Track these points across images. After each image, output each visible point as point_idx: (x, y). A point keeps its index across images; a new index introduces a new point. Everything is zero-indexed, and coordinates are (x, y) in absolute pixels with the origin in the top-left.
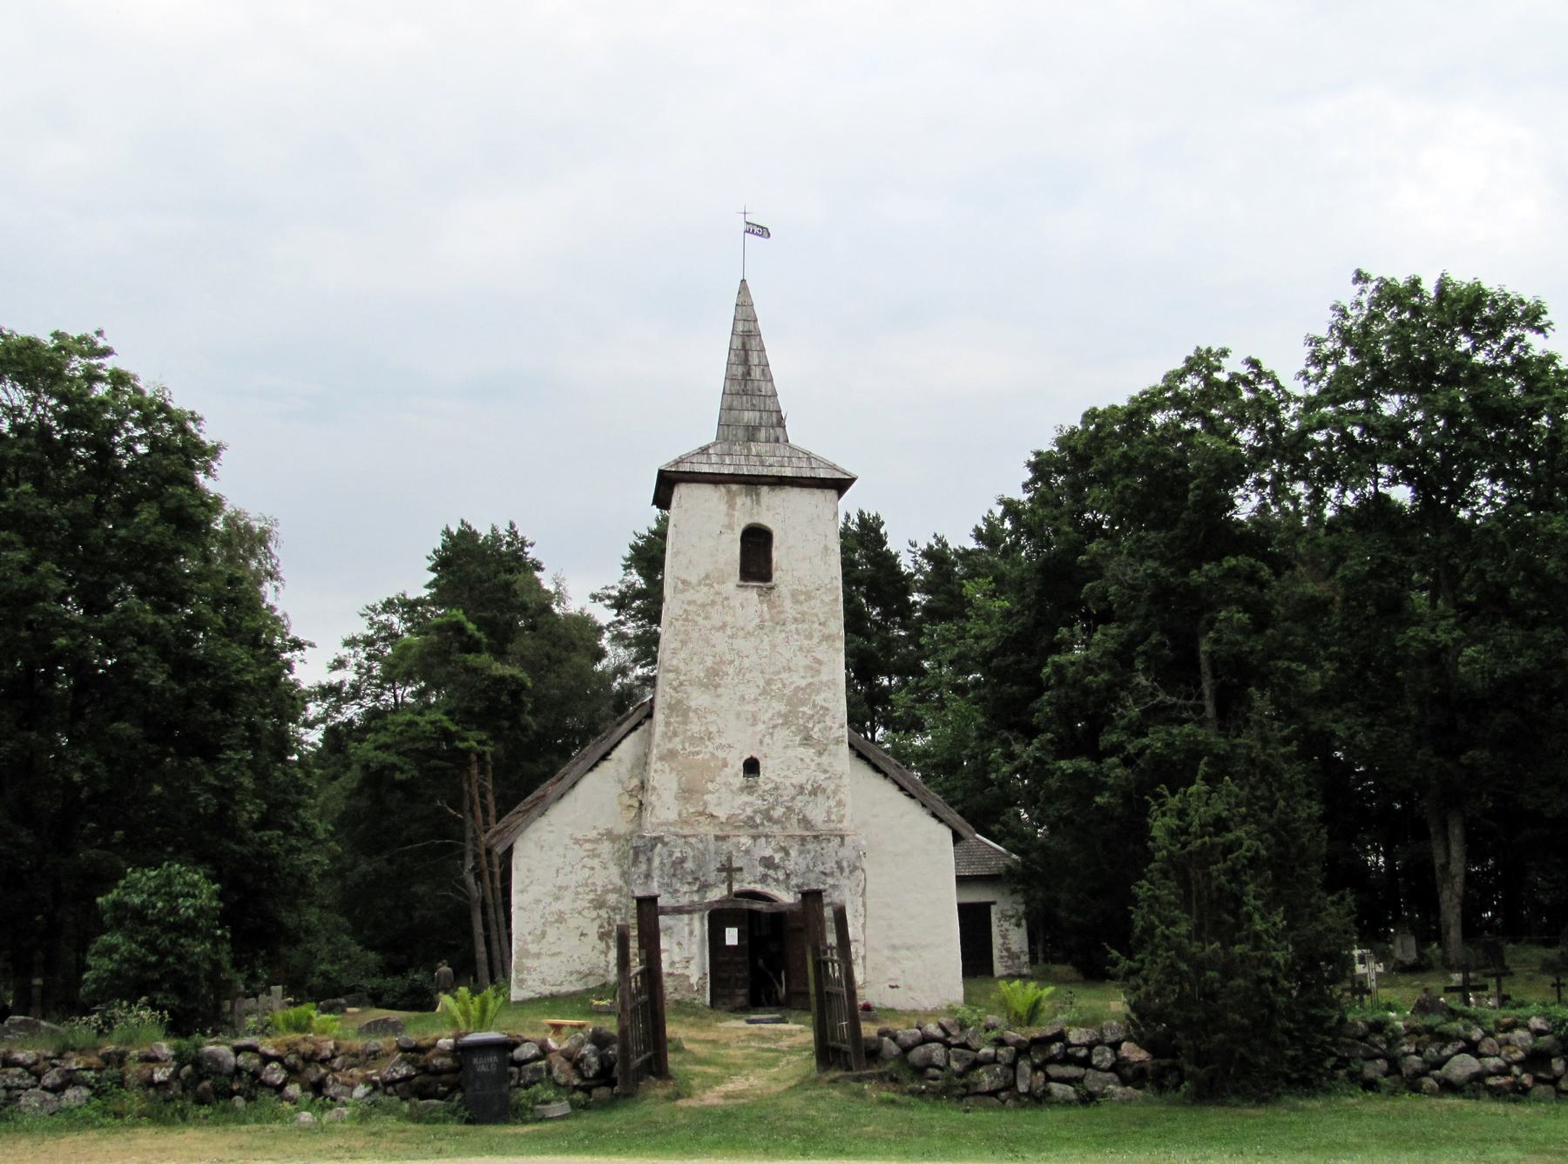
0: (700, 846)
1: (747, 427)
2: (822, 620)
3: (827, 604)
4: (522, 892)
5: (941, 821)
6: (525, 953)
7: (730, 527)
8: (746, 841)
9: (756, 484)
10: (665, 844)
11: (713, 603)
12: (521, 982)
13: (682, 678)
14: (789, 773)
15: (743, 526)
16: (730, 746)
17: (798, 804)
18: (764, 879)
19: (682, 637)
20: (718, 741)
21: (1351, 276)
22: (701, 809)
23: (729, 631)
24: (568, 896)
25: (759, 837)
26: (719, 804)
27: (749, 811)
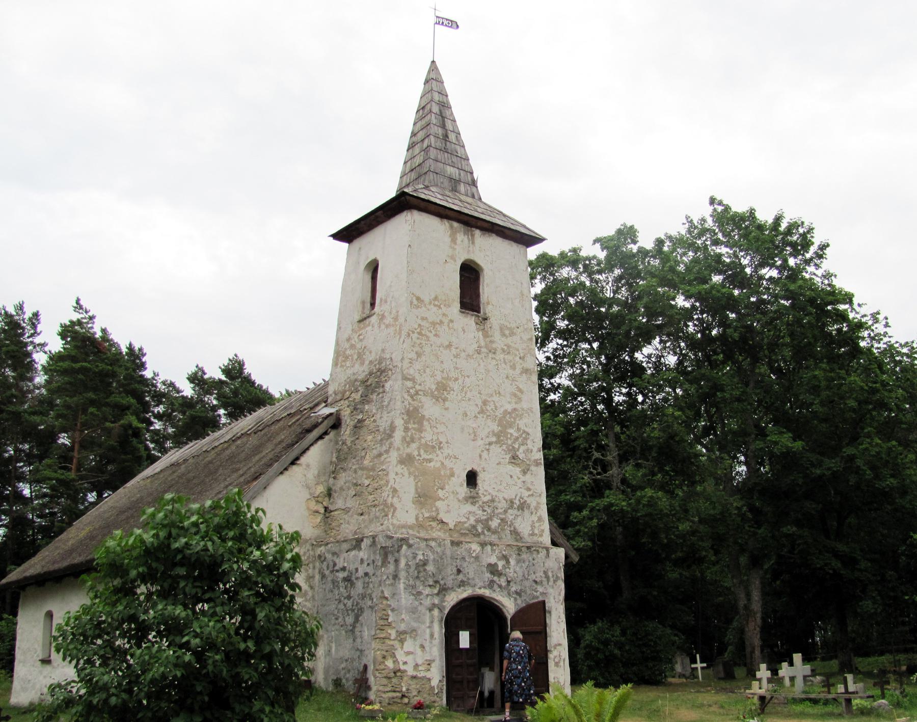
2: (522, 355)
7: (453, 258)
10: (410, 546)
13: (418, 387)
16: (455, 458)
18: (491, 585)
19: (417, 349)
21: (707, 201)
22: (434, 514)
23: (454, 351)
26: (448, 512)
27: (472, 521)
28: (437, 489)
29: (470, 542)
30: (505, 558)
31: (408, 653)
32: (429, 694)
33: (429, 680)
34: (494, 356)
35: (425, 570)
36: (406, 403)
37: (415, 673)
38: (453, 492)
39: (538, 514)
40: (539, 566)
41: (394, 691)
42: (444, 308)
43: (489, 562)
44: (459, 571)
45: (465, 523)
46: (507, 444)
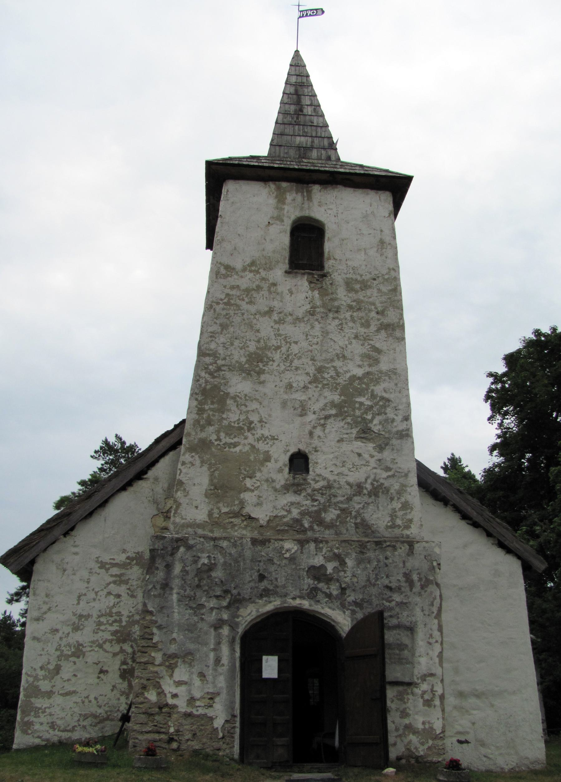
0: (233, 551)
1: (299, 147)
2: (380, 309)
3: (385, 294)
4: (37, 619)
5: (509, 551)
6: (36, 691)
7: (279, 219)
8: (290, 546)
9: (308, 182)
10: (189, 548)
11: (259, 288)
12: (28, 725)
13: (220, 362)
14: (345, 470)
15: (293, 217)
17: (356, 504)
18: (312, 593)
19: (222, 320)
20: (259, 432)
22: (236, 508)
23: (275, 317)
24: (90, 625)
25: (307, 541)
26: (259, 504)
27: (295, 513)
28: (244, 478)
29: (282, 540)
30: (340, 559)
31: (179, 683)
32: (211, 738)
33: (211, 719)
34: (336, 315)
35: (209, 577)
36: (202, 381)
37: (189, 710)
38: (267, 480)
39: (403, 499)
40: (396, 567)
41: (159, 733)
42: (263, 273)
43: (311, 564)
44: (262, 577)
45: (284, 517)
46: (354, 415)
